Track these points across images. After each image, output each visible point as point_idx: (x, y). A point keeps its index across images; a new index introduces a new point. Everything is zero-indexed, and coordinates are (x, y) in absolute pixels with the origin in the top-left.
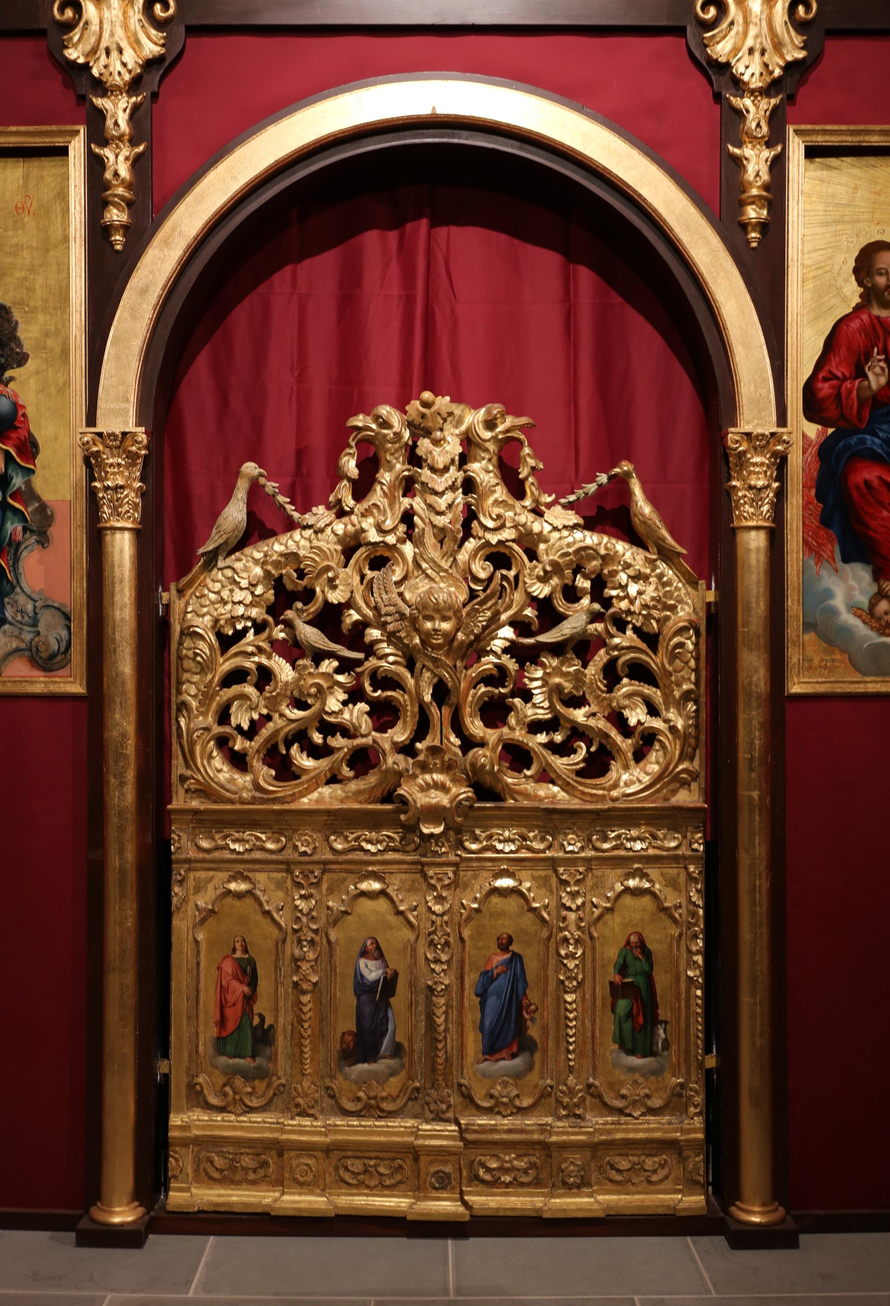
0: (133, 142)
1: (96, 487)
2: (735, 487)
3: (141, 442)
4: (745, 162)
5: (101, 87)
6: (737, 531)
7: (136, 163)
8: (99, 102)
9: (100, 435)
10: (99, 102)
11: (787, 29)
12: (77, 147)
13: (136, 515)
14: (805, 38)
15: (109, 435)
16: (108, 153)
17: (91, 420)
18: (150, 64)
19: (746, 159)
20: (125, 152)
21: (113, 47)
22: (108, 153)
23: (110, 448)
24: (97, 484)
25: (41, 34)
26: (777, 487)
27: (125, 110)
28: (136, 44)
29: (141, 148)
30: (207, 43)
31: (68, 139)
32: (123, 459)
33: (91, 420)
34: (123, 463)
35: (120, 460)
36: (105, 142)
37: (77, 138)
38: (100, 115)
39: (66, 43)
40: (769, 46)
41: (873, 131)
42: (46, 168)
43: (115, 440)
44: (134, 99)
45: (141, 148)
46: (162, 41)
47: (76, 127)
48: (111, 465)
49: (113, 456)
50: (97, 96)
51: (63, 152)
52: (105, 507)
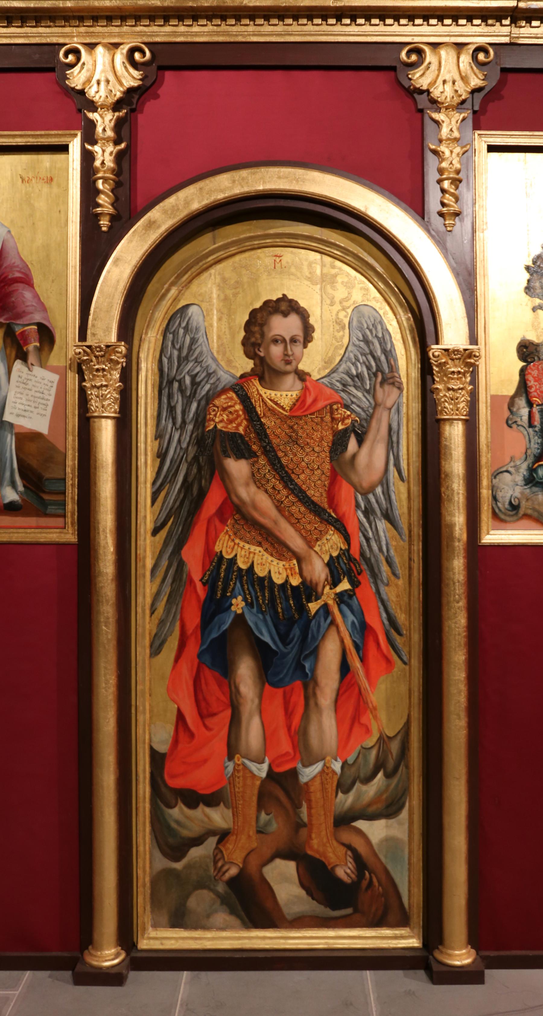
0: (117, 142)
1: (85, 386)
2: (437, 389)
3: (121, 353)
4: (95, 154)
5: (92, 106)
6: (92, 420)
7: (119, 157)
8: (91, 115)
9: (89, 347)
10: (91, 115)
11: (126, 67)
12: (75, 146)
13: (116, 407)
14: (141, 72)
15: (454, 351)
16: (97, 149)
17: (83, 336)
18: (130, 91)
19: (96, 152)
20: (110, 148)
21: (103, 79)
22: (97, 149)
23: (452, 360)
24: (88, 385)
25: (52, 70)
26: (471, 389)
27: (111, 120)
28: (464, 79)
29: (123, 145)
30: (511, 76)
31: (69, 139)
32: (462, 369)
33: (83, 336)
34: (462, 371)
35: (104, 366)
36: (94, 142)
37: (75, 140)
38: (92, 125)
39: (68, 76)
40: (457, 77)
41: (52, 135)
42: (59, 157)
43: (101, 351)
44: (117, 114)
45: (123, 145)
46: (140, 77)
47: (76, 132)
48: (453, 373)
49: (456, 366)
50: (89, 111)
51: (64, 149)
52: (93, 401)
